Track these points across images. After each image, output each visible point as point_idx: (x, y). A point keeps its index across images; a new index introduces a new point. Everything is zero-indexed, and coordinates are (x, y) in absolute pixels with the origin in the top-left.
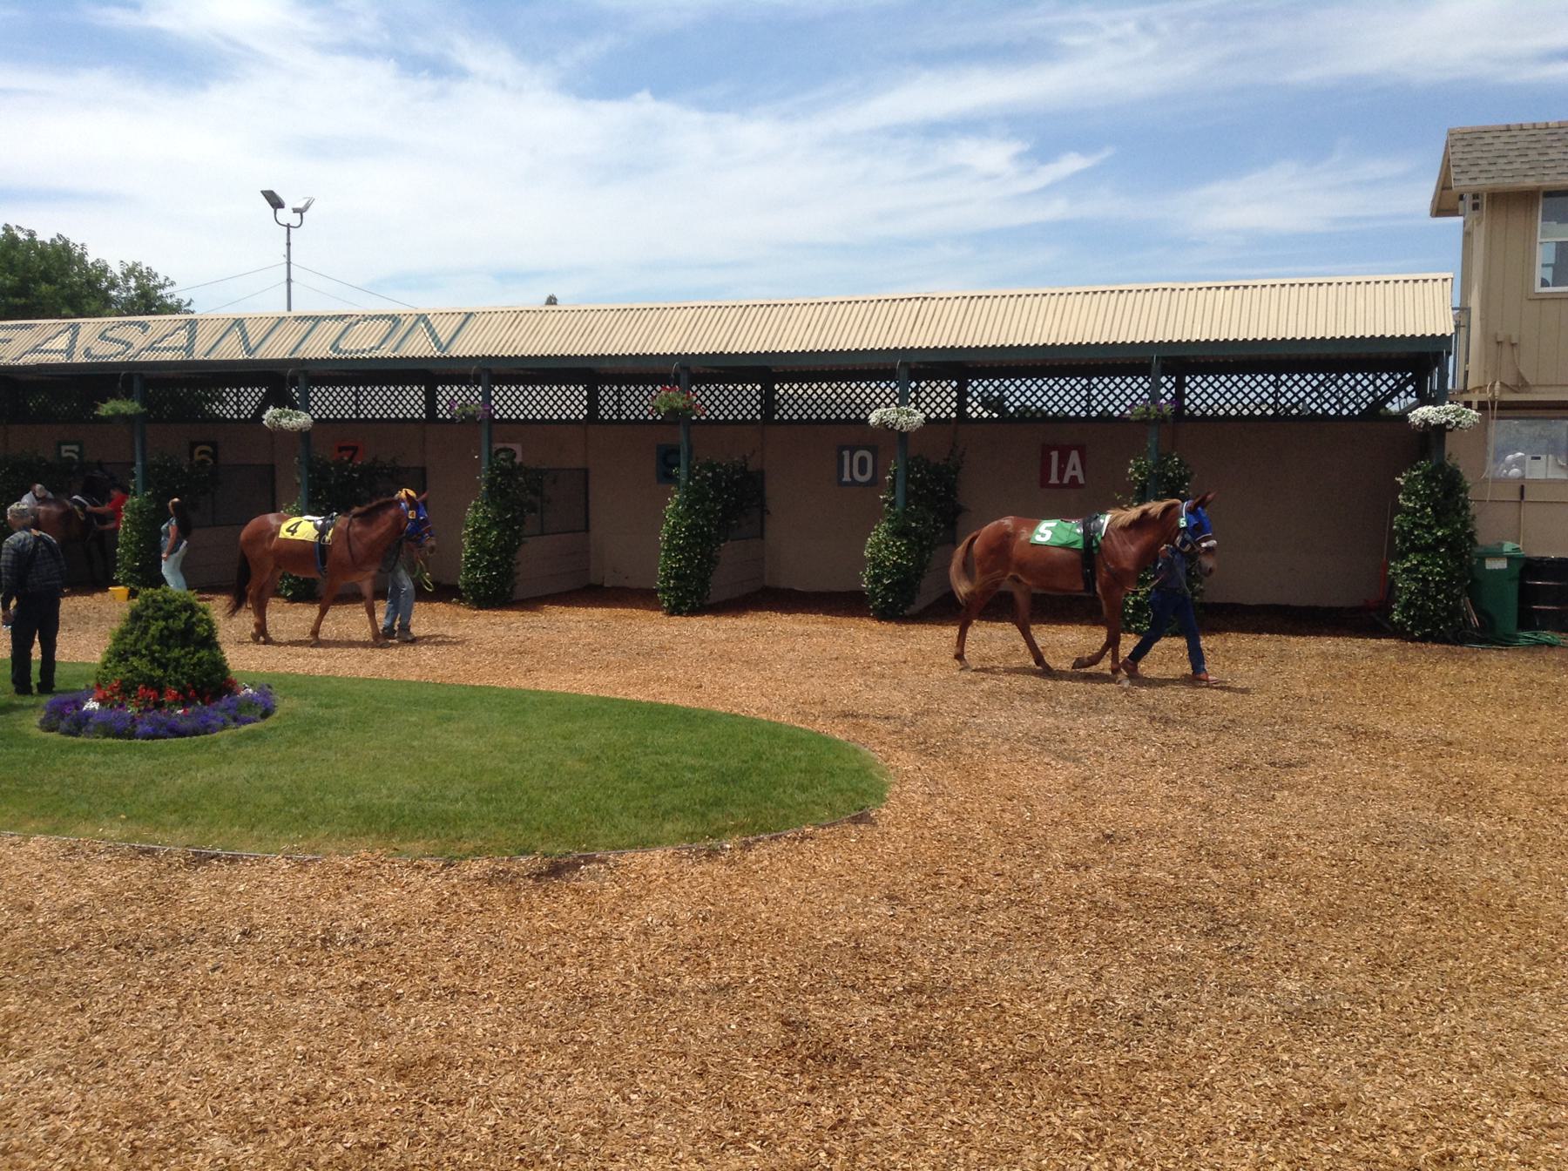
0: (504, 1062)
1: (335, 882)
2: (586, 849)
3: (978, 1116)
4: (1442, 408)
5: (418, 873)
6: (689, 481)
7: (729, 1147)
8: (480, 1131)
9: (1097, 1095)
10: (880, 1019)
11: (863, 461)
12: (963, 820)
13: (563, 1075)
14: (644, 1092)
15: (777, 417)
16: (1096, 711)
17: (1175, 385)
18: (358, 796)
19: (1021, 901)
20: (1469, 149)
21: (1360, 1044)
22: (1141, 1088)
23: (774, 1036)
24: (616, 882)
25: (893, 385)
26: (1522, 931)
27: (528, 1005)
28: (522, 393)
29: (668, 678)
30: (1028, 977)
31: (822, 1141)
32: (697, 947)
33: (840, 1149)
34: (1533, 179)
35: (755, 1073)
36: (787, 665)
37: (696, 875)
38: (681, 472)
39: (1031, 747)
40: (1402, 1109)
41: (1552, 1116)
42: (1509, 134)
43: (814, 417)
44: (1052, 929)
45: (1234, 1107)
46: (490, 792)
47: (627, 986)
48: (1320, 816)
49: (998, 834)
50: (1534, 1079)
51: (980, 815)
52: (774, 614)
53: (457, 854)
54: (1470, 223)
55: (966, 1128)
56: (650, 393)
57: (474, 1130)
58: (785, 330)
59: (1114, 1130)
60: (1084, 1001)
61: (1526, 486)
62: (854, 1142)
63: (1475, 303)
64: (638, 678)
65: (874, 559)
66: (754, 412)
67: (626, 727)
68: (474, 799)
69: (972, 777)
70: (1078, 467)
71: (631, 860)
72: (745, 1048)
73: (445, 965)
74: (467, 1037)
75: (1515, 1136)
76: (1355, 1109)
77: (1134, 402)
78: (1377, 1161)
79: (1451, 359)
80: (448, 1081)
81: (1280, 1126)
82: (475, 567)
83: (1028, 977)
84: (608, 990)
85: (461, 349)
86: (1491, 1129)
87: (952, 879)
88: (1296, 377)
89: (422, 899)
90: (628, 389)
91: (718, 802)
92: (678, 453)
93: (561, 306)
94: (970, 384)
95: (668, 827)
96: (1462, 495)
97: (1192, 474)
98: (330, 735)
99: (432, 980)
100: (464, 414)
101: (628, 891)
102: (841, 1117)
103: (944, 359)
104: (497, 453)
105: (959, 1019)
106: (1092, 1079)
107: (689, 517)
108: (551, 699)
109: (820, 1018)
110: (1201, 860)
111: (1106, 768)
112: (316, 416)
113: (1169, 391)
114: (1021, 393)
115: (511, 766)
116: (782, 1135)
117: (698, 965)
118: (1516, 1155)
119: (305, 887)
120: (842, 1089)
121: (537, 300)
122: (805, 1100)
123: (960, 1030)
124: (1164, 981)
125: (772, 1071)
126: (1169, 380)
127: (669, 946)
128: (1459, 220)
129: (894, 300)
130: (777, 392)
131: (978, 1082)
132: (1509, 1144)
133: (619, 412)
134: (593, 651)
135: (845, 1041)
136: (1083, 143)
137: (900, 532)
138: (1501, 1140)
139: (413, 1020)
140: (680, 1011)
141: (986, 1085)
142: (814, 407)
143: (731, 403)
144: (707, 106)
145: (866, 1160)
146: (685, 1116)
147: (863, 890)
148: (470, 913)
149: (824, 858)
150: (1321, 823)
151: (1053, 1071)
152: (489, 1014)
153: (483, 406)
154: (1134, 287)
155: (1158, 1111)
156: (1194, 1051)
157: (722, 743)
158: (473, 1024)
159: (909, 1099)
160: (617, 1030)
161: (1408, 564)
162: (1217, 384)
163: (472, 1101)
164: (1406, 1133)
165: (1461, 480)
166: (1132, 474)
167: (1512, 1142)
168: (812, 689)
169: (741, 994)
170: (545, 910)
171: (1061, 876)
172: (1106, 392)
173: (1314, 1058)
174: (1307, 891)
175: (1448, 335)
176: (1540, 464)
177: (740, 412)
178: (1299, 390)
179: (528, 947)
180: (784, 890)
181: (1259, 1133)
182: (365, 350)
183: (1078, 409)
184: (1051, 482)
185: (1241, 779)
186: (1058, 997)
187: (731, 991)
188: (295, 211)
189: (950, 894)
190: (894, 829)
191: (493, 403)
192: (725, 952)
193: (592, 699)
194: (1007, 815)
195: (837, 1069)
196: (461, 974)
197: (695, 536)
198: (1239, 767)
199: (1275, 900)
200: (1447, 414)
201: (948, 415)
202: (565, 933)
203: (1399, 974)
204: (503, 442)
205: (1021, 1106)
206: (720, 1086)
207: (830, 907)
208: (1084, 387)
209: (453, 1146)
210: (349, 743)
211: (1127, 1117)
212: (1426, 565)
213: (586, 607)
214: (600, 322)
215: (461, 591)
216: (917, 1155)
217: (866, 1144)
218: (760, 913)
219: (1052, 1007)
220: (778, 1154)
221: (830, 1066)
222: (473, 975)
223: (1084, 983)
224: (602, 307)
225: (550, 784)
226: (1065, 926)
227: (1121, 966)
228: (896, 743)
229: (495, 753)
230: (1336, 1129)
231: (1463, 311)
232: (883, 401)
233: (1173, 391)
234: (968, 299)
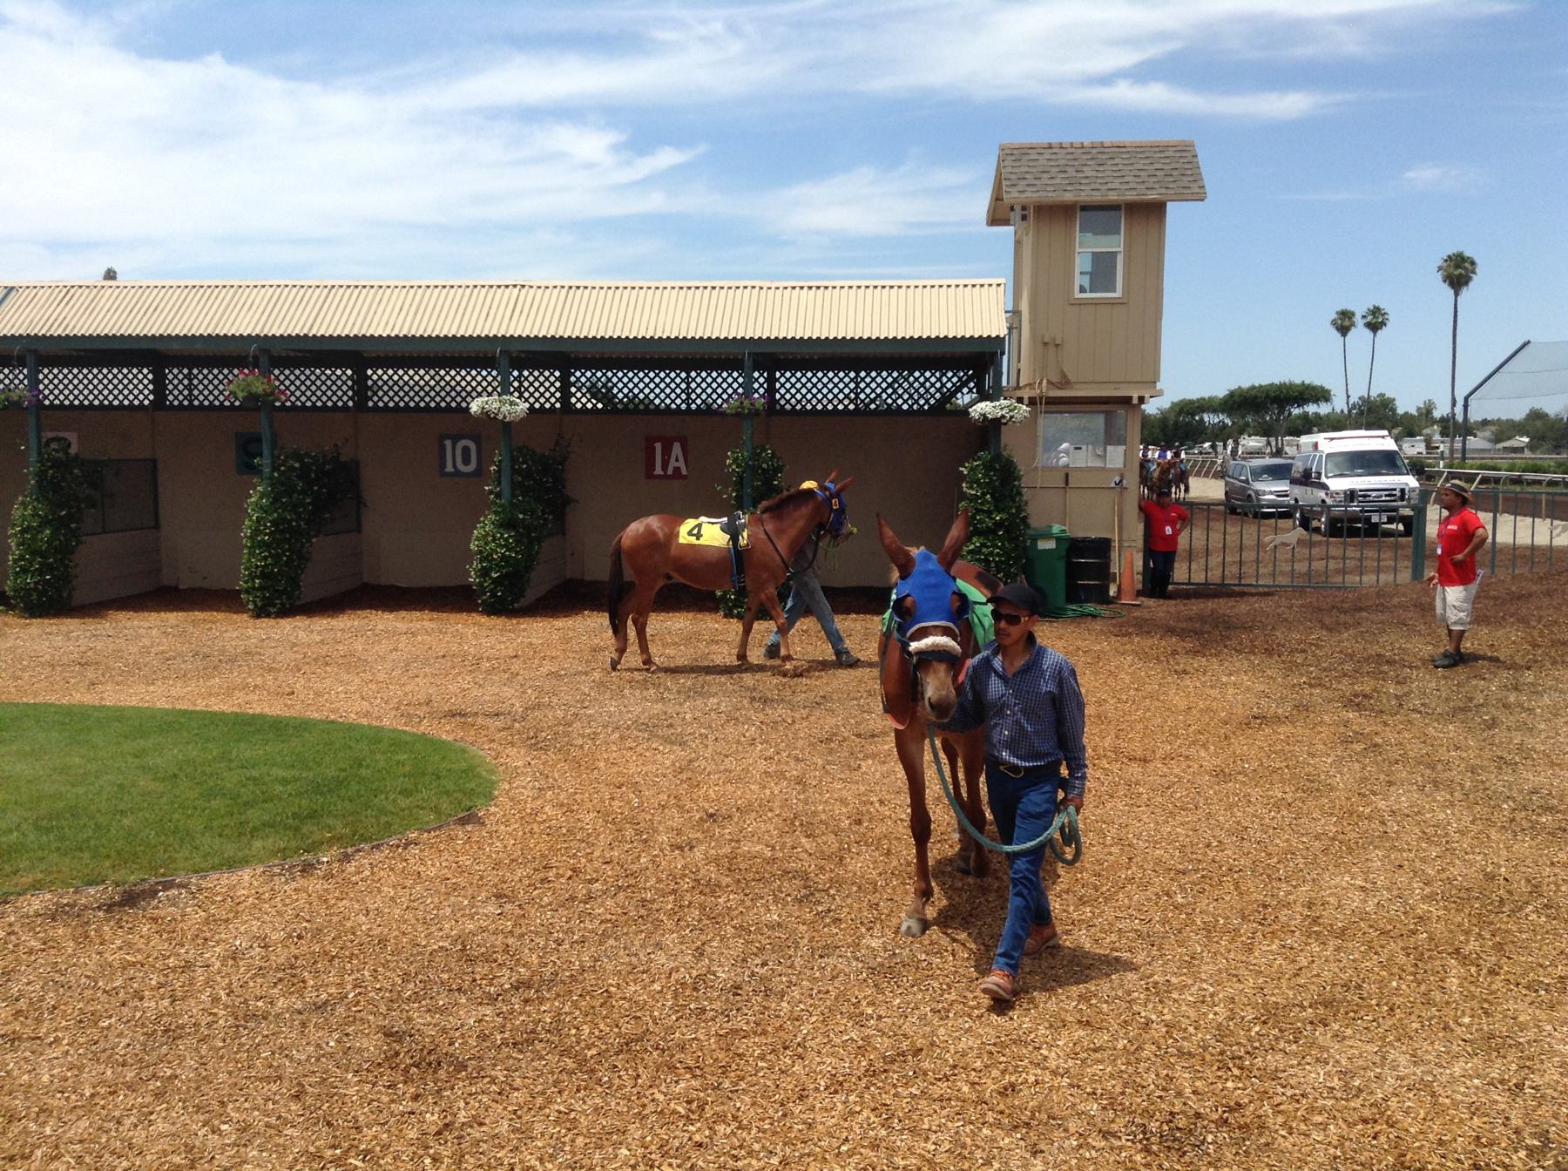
0: (75, 1107)
3: (585, 1102)
4: (997, 403)
6: (273, 471)
7: (328, 1166)
9: (698, 1067)
10: (487, 1019)
11: (466, 450)
12: (572, 811)
13: (143, 1114)
14: (235, 1120)
16: (701, 694)
19: (628, 886)
21: (935, 992)
22: (739, 1055)
23: (376, 1049)
24: (200, 907)
27: (102, 1045)
28: (95, 376)
30: (634, 960)
31: (427, 1148)
32: (292, 967)
33: (445, 1153)
35: (356, 1088)
37: (289, 892)
38: (264, 462)
41: (1096, 1041)
42: (1050, 151)
44: (657, 911)
45: (824, 1063)
46: (50, 820)
48: (899, 781)
49: (607, 822)
52: (374, 612)
53: (13, 890)
59: (715, 1099)
62: (459, 1144)
63: (1024, 307)
64: (220, 687)
65: (480, 552)
67: (207, 740)
68: (31, 827)
69: (582, 768)
70: (681, 458)
71: (216, 882)
74: (31, 1086)
75: (1066, 1062)
76: (931, 1053)
77: (730, 396)
78: (949, 1099)
79: (1005, 358)
80: (10, 1135)
81: (865, 1076)
82: (24, 570)
83: (634, 960)
84: (193, 1021)
86: (1046, 1058)
87: (561, 872)
88: (874, 374)
91: (313, 815)
92: (259, 440)
93: (120, 282)
94: (573, 374)
95: (258, 844)
96: (1016, 483)
101: (214, 915)
102: (447, 1121)
104: (47, 443)
105: (566, 1009)
106: (694, 1052)
107: (275, 511)
108: (118, 715)
109: (424, 1025)
111: (710, 750)
113: (761, 385)
114: (628, 385)
115: (74, 790)
116: (385, 1147)
117: (293, 985)
118: (1068, 1080)
120: (448, 1093)
121: (95, 274)
122: (409, 1109)
123: (567, 1020)
124: (762, 949)
125: (374, 1085)
126: (761, 375)
127: (260, 969)
128: (1010, 229)
129: (491, 287)
131: (585, 1069)
132: (1061, 1070)
134: (169, 659)
135: (450, 1045)
137: (508, 524)
138: (1054, 1067)
141: (593, 1071)
142: (319, 393)
144: (289, 74)
145: (472, 1160)
146: (281, 1141)
147: (470, 891)
148: (30, 953)
150: (900, 788)
151: (657, 1049)
152: (57, 1058)
153: (30, 391)
154: (725, 284)
155: (755, 1075)
156: (788, 1014)
158: (38, 1071)
159: (516, 1094)
161: (972, 547)
164: (974, 1070)
166: (730, 465)
167: (1064, 1068)
168: (417, 689)
169: (341, 1010)
170: (119, 942)
171: (667, 858)
172: (704, 385)
173: (895, 1008)
175: (1002, 336)
176: (1082, 454)
178: (876, 386)
179: (100, 984)
183: (678, 401)
184: (446, 470)
185: (831, 751)
186: (663, 976)
189: (559, 887)
191: (41, 387)
192: (322, 969)
193: (166, 712)
194: (616, 803)
195: (442, 1074)
197: (282, 532)
198: (829, 740)
201: (553, 405)
204: (54, 430)
205: (626, 1087)
206: (318, 1105)
207: (435, 912)
208: (852, 380)
211: (727, 1084)
212: (987, 547)
213: (158, 611)
215: (9, 598)
216: (524, 1149)
217: (472, 1145)
218: (360, 925)
219: (657, 987)
220: (381, 1166)
222: (36, 1019)
225: (121, 807)
226: (670, 906)
227: (721, 940)
228: (506, 739)
229: (54, 777)
231: (1015, 314)
233: (765, 386)
234: (567, 288)
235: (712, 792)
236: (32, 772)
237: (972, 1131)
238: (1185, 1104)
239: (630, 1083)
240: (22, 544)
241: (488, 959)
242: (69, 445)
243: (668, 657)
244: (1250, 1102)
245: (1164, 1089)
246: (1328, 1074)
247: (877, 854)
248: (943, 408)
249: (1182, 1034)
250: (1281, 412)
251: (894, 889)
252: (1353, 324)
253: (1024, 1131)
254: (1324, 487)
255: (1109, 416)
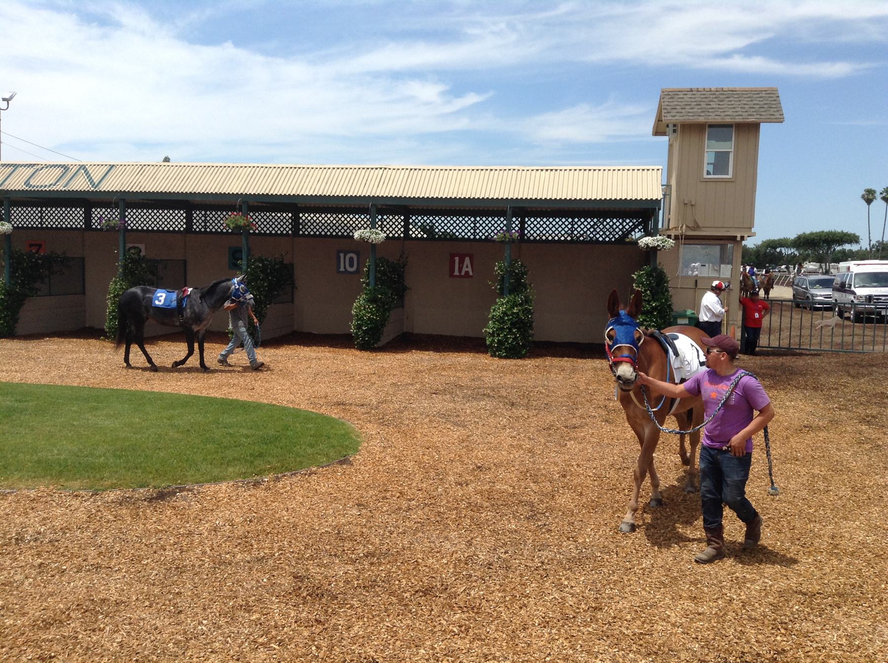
1: (24, 505)
2: (180, 484)
4: (655, 238)
5: (76, 499)
7: (260, 647)
8: (112, 645)
10: (350, 572)
11: (351, 259)
15: (301, 233)
17: (520, 223)
18: (39, 454)
19: (431, 504)
20: (671, 100)
21: (605, 575)
24: (198, 502)
25: (368, 217)
26: (689, 513)
27: (143, 573)
29: (234, 384)
32: (246, 537)
33: (324, 644)
34: (704, 118)
35: (277, 605)
36: (305, 376)
38: (243, 263)
39: (441, 420)
40: (625, 608)
42: (691, 93)
43: (340, 234)
44: (447, 518)
47: (203, 561)
49: (420, 467)
50: (692, 590)
51: (411, 457)
52: (299, 347)
53: (100, 488)
54: (671, 141)
55: (395, 629)
56: (224, 216)
57: (108, 645)
58: (305, 182)
60: (462, 556)
61: (698, 280)
63: (673, 183)
64: (215, 384)
65: (357, 315)
66: (287, 229)
71: (207, 489)
72: (271, 592)
73: (92, 552)
77: (498, 231)
79: (661, 212)
85: (106, 186)
86: (669, 616)
88: (583, 220)
89: (78, 514)
90: (211, 213)
91: (261, 455)
94: (411, 218)
95: (231, 469)
96: (666, 285)
97: (528, 271)
98: (22, 419)
99: (84, 561)
100: (108, 225)
101: (205, 507)
103: (395, 203)
104: (129, 250)
109: (315, 573)
110: (527, 479)
112: (15, 225)
114: (443, 224)
115: (135, 436)
117: (246, 547)
119: (5, 508)
121: (158, 159)
123: (394, 576)
124: (505, 544)
126: (517, 220)
127: (229, 537)
130: (301, 218)
131: (404, 603)
132: (678, 624)
133: (205, 226)
135: (329, 585)
136: (478, 88)
137: (372, 300)
138: (673, 622)
139: (72, 584)
140: (234, 573)
142: (323, 227)
143: (273, 223)
147: (344, 501)
148: (108, 522)
149: (322, 484)
152: (119, 579)
154: (498, 168)
157: (265, 421)
160: (196, 585)
162: (542, 223)
163: (108, 628)
165: (665, 276)
166: (497, 270)
167: (679, 623)
168: (320, 389)
169: (271, 562)
170: (154, 519)
174: (581, 494)
175: (659, 199)
176: (705, 269)
177: (279, 229)
178: (584, 227)
179: (144, 541)
180: (298, 503)
181: (550, 623)
182: (46, 185)
183: (469, 234)
185: (550, 435)
186: (448, 555)
187: (265, 561)
188: (4, 100)
190: (363, 467)
193: (186, 396)
196: (102, 557)
199: (564, 499)
200: (658, 241)
202: (166, 532)
203: (626, 537)
205: (425, 615)
207: (324, 512)
209: (96, 654)
210: (34, 423)
212: (647, 321)
214: (193, 174)
216: (367, 645)
218: (283, 517)
219: (445, 561)
220: (288, 649)
221: (320, 600)
222: (109, 557)
223: (462, 547)
224: (195, 165)
225: (159, 446)
226: (454, 517)
227: (482, 537)
230: (591, 619)
231: (667, 187)
232: (362, 225)
233: (519, 226)
235: (480, 454)
236: (113, 425)
237: (623, 655)
238: (751, 648)
239: (427, 613)
240: (114, 303)
241: (352, 539)
242: (140, 251)
243: (458, 377)
244: (791, 649)
245: (739, 638)
246: (840, 636)
247: (574, 494)
248: (623, 240)
249: (751, 607)
250: (829, 248)
251: (583, 515)
252: (875, 198)
253: (654, 657)
254: (853, 293)
255: (723, 249)
